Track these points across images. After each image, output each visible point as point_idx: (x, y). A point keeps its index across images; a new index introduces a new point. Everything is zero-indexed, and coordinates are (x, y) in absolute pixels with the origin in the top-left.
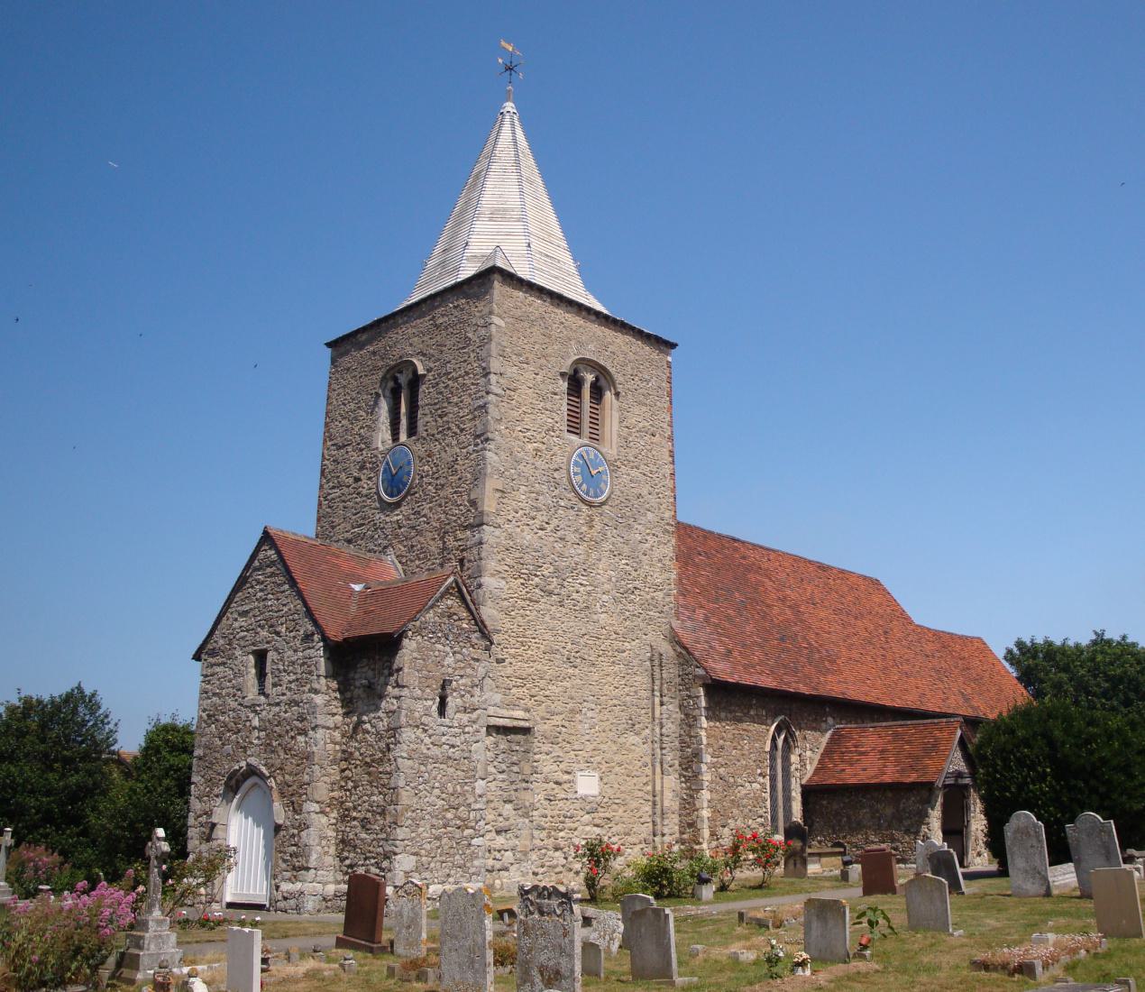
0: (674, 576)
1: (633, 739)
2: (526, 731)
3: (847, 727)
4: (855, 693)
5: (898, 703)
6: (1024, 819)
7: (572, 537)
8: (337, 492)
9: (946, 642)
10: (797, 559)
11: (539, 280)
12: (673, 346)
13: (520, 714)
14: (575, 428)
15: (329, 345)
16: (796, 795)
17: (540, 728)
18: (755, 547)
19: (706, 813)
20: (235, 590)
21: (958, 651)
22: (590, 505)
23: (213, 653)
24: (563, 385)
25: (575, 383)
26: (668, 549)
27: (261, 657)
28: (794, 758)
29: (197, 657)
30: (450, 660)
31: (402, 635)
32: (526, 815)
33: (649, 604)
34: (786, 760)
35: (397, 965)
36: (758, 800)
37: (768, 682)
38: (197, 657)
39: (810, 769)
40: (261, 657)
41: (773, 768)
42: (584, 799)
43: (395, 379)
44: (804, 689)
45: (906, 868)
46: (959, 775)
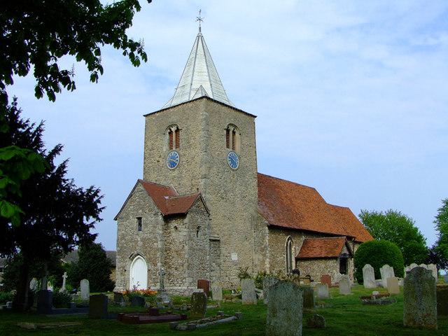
0: (257, 191)
1: (247, 243)
2: (219, 240)
3: (309, 238)
4: (311, 228)
5: (324, 231)
6: (368, 266)
7: (229, 181)
8: (150, 165)
9: (337, 209)
10: (289, 182)
11: (216, 99)
12: (256, 117)
13: (216, 236)
14: (228, 146)
15: (144, 116)
16: (293, 260)
17: (222, 240)
18: (277, 179)
19: (268, 266)
20: (128, 199)
21: (342, 213)
22: (233, 170)
23: (122, 218)
24: (225, 132)
25: (228, 131)
26: (255, 183)
27: (140, 219)
28: (293, 249)
29: (116, 219)
30: (199, 220)
31: (187, 213)
32: (219, 266)
33: (250, 201)
34: (290, 249)
35: (313, 285)
36: (283, 262)
37: (285, 225)
38: (116, 219)
39: (298, 252)
40: (140, 219)
41: (287, 252)
42: (233, 261)
43: (170, 130)
44: (296, 227)
45: (39, 328)
46: (345, 254)
